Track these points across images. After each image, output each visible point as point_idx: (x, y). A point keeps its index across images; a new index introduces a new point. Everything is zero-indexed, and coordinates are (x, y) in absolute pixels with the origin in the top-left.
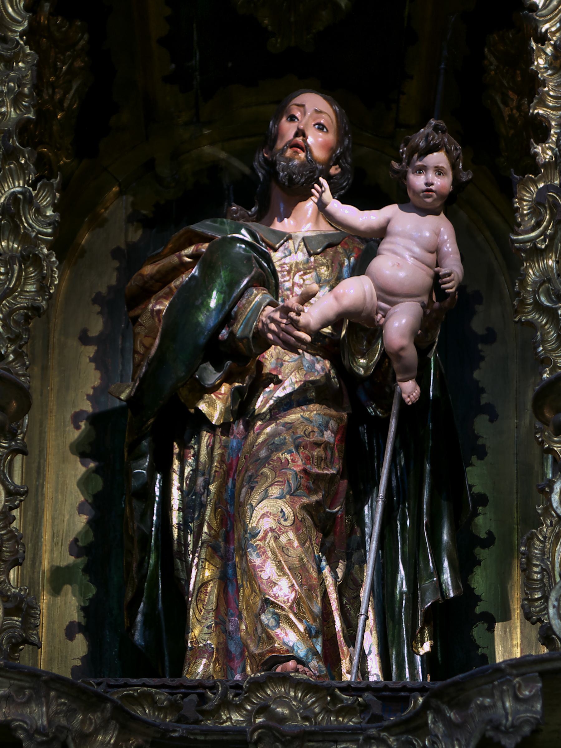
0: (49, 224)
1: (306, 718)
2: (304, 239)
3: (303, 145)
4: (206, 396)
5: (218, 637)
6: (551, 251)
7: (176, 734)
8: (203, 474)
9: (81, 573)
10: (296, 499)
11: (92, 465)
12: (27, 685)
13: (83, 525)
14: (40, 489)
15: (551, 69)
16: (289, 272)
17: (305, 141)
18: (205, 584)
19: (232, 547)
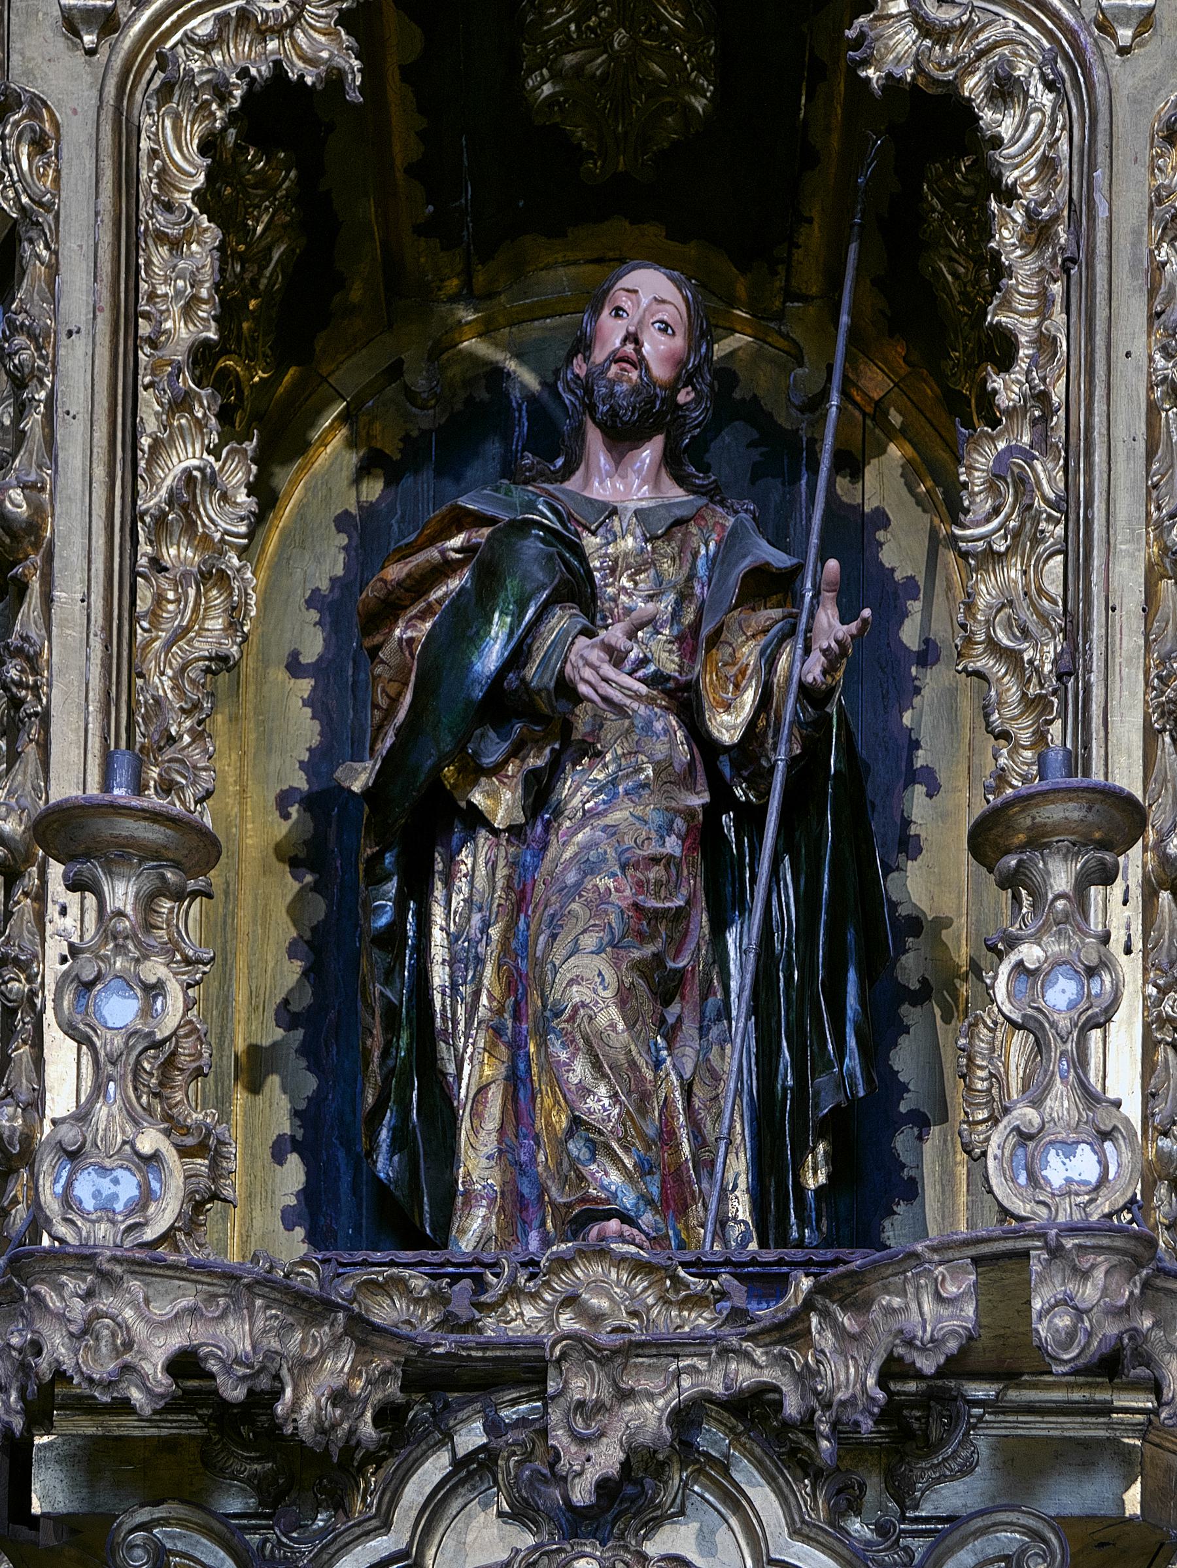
0: (242, 519)
1: (634, 1314)
2: (637, 513)
3: (634, 357)
4: (483, 780)
5: (504, 1172)
6: (1015, 554)
7: (441, 1350)
8: (480, 910)
9: (293, 1056)
10: (622, 952)
11: (309, 878)
12: (222, 1291)
13: (296, 976)
14: (229, 921)
15: (1022, 248)
16: (613, 570)
17: (638, 351)
18: (482, 1089)
19: (524, 1026)
